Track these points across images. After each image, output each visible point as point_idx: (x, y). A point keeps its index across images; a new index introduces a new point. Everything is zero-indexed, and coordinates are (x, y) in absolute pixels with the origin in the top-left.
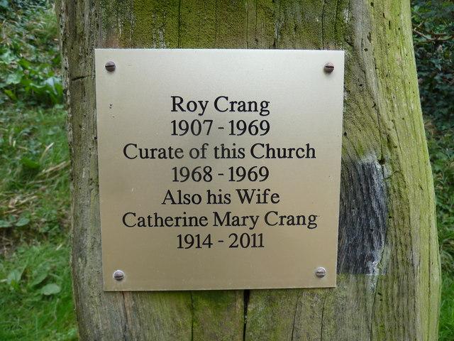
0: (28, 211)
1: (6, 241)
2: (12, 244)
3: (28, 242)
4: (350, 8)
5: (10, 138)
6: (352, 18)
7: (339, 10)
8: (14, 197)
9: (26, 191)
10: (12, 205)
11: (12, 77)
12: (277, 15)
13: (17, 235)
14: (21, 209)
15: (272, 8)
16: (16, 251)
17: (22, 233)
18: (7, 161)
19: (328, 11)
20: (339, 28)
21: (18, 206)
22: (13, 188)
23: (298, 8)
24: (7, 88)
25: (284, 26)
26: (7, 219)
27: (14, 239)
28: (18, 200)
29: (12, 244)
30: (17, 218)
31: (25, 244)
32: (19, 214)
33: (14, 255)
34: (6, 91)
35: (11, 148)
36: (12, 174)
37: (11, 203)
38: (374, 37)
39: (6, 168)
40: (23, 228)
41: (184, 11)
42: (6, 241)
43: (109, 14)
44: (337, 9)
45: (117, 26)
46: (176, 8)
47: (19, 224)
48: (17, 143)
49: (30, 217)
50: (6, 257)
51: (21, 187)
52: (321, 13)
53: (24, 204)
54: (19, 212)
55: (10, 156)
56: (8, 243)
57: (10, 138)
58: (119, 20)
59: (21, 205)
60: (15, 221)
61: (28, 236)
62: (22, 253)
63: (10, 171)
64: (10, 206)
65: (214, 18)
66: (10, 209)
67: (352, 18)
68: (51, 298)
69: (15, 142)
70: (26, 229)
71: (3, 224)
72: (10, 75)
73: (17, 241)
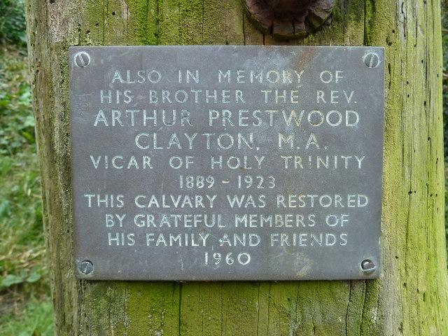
0: (39, 266)
1: (17, 297)
2: (23, 299)
3: (38, 298)
4: (379, 305)
5: (26, 186)
6: (382, 317)
7: (366, 308)
8: (27, 250)
9: (38, 244)
10: (24, 259)
11: (29, 120)
12: (293, 316)
13: (28, 291)
14: (33, 263)
15: (287, 307)
16: (26, 307)
17: (33, 288)
18: (22, 210)
19: (353, 309)
20: (365, 328)
21: (30, 260)
22: (24, 241)
23: (317, 307)
24: (24, 130)
25: (302, 327)
26: (19, 273)
27: (25, 294)
28: (31, 254)
29: (23, 299)
30: (28, 272)
31: (35, 300)
32: (31, 268)
33: (24, 312)
34: (24, 133)
35: (26, 196)
36: (26, 224)
37: (23, 257)
38: (406, 326)
39: (20, 217)
40: (34, 284)
41: (185, 310)
42: (17, 297)
43: (101, 316)
44: (364, 307)
45: (109, 328)
46: (176, 308)
47: (30, 280)
48: (32, 192)
49: (41, 272)
50: (17, 313)
51: (33, 240)
52: (344, 313)
53: (36, 258)
54: (31, 266)
55: (24, 205)
56: (19, 299)
57: (26, 186)
58: (111, 322)
59: (33, 259)
60: (26, 276)
61: (39, 292)
62: (32, 311)
63: (24, 222)
64: (22, 261)
65: (220, 319)
66: (22, 264)
67: (382, 317)
68: (66, 183)
69: (29, 191)
70: (37, 284)
71: (15, 279)
72: (28, 117)
73: (28, 297)
